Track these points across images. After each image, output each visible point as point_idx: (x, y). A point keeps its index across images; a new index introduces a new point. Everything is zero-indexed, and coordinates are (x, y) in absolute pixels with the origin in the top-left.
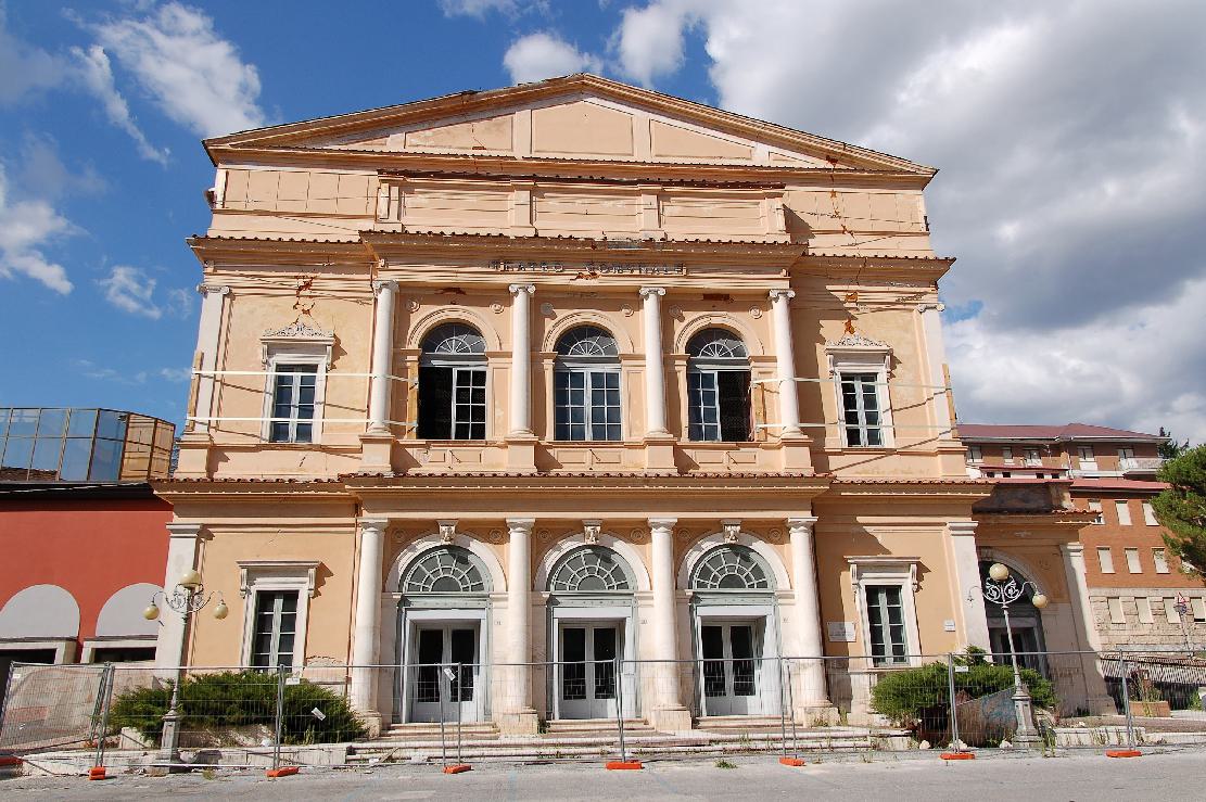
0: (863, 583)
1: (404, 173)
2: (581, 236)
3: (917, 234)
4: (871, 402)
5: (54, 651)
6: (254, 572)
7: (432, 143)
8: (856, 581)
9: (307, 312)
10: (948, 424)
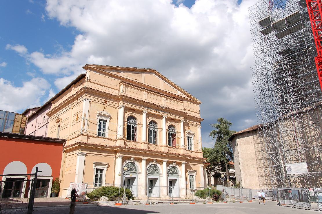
0: (189, 174)
1: (127, 83)
2: (157, 104)
3: (197, 113)
4: (104, 126)
5: (49, 180)
6: (97, 164)
7: (128, 76)
8: (94, 167)
9: (105, 108)
10: (201, 148)
